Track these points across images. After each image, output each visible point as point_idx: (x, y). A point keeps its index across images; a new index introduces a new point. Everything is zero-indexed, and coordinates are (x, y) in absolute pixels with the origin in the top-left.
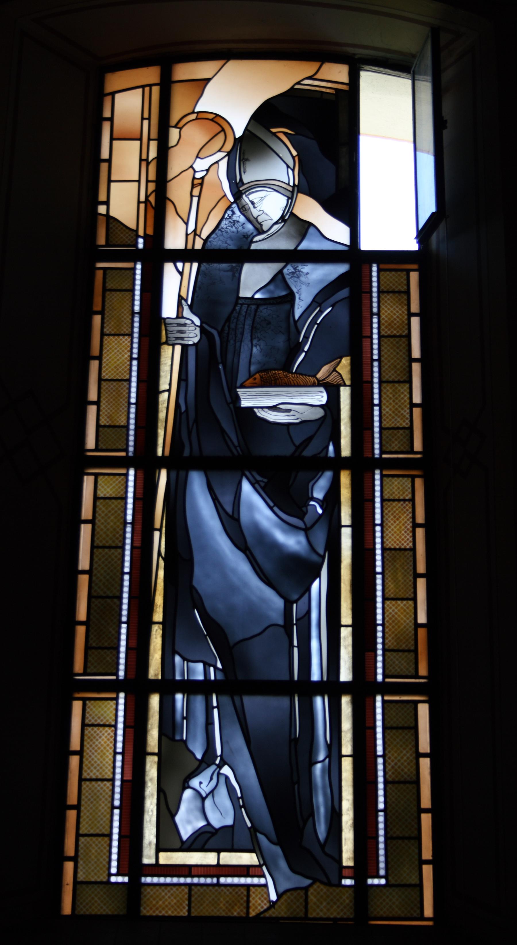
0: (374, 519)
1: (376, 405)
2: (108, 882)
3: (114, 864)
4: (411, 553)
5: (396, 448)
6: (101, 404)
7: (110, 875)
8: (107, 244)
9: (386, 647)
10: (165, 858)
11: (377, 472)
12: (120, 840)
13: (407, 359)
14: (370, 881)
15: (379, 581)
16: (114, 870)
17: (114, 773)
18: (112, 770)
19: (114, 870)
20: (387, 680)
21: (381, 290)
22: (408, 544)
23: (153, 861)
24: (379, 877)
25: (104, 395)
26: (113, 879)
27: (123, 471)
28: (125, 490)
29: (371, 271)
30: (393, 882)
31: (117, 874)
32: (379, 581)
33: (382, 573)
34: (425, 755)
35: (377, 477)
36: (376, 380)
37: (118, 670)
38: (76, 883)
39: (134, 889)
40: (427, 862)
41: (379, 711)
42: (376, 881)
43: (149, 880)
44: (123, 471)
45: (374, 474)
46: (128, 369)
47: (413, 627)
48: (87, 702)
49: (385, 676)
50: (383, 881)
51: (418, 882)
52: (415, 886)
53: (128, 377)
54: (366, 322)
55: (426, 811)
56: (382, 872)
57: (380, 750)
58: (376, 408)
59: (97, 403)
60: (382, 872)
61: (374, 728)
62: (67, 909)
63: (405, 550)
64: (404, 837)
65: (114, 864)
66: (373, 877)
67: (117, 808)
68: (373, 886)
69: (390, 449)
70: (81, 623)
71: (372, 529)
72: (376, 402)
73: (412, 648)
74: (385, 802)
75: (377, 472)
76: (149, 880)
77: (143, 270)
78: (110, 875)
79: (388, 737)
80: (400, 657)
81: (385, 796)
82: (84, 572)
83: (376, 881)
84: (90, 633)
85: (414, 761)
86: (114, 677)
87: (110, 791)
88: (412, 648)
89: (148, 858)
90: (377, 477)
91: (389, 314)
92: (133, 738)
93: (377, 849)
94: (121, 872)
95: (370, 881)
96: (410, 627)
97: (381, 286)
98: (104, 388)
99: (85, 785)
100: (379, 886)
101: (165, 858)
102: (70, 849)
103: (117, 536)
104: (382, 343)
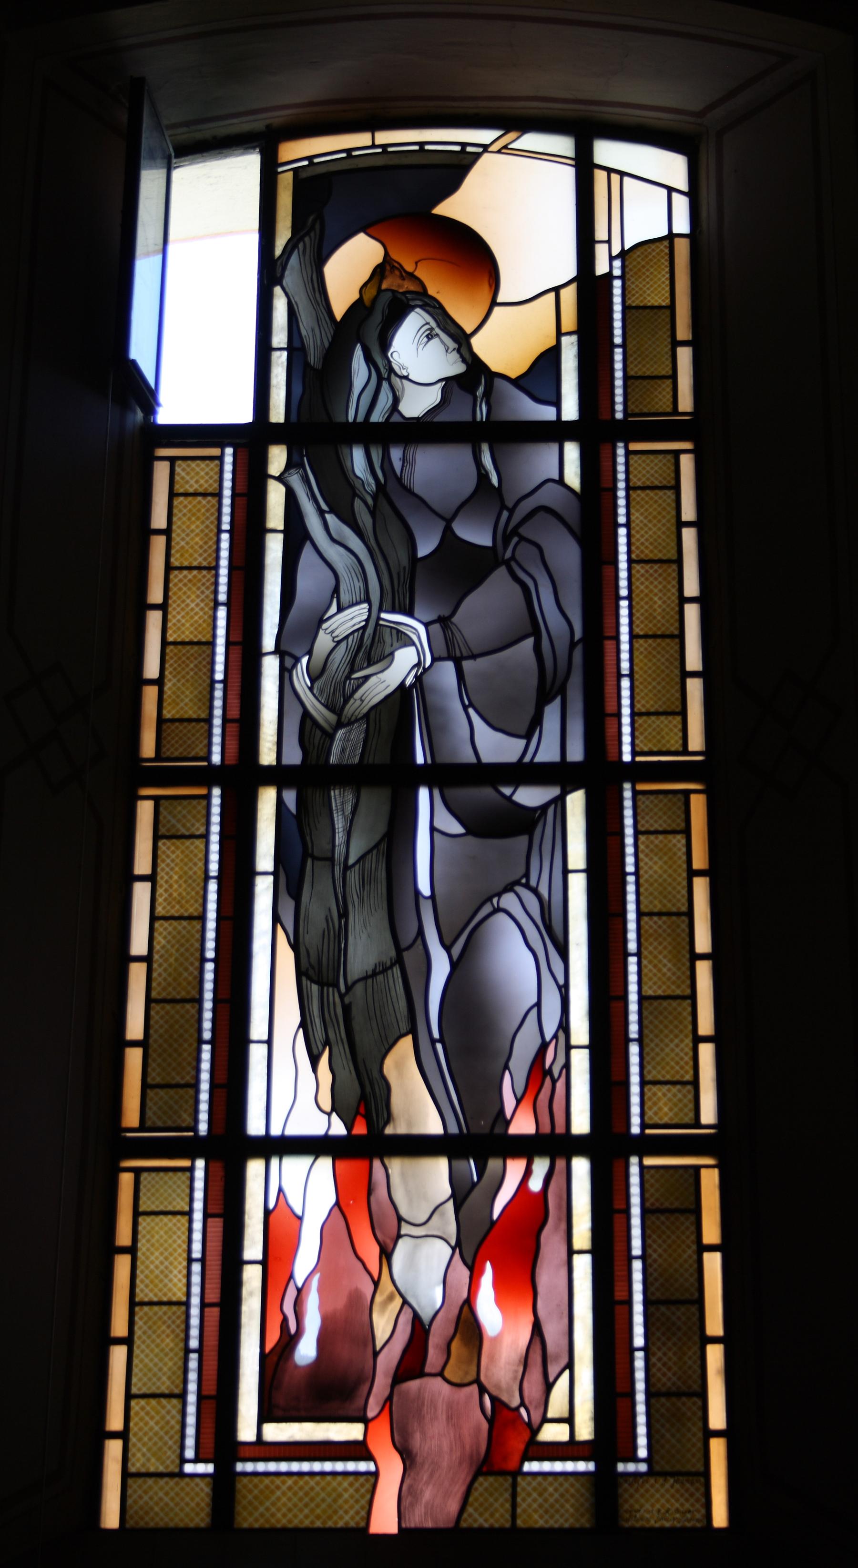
0: (617, 587)
1: (618, 346)
2: (182, 1475)
3: (190, 1442)
4: (668, 312)
5: (666, 1120)
6: (170, 609)
7: (183, 1461)
8: (158, 757)
9: (633, 556)
10: (275, 1432)
11: (627, 786)
12: (214, 1010)
13: (674, 521)
14: (621, 1467)
15: (633, 968)
16: (190, 1453)
17: (188, 1294)
18: (185, 1289)
19: (190, 1453)
20: (638, 759)
21: (636, 710)
22: (669, 497)
23: (262, 1132)
24: (636, 1459)
25: (174, 617)
26: (189, 1468)
27: (186, 1163)
28: (215, 547)
29: (614, 456)
30: (657, 1468)
31: (197, 1460)
32: (633, 968)
33: (638, 954)
34: (712, 1248)
35: (628, 794)
36: (621, 485)
37: (196, 1121)
38: (161, 721)
39: (224, 1483)
40: (694, 674)
41: (635, 1190)
42: (631, 1467)
43: (249, 1467)
44: (186, 1163)
45: (621, 791)
46: (211, 584)
47: (677, 601)
48: (137, 1300)
49: (634, 753)
50: (643, 1467)
51: (702, 1469)
52: (697, 1474)
53: (202, 830)
54: (609, 688)
55: (718, 1434)
56: (642, 1453)
57: (637, 1247)
58: (633, 960)
59: (151, 878)
60: (642, 1453)
61: (626, 1212)
62: (111, 1518)
63: (660, 307)
64: (679, 1395)
65: (190, 1442)
66: (626, 1460)
67: (207, 1042)
68: (626, 1475)
69: (656, 1120)
70: (134, 1044)
71: (615, 683)
72: (622, 520)
73: (684, 909)
74: (650, 1447)
75: (627, 786)
76: (249, 1467)
77: (223, 797)
78: (183, 1461)
79: (648, 1223)
80: (656, 571)
81: (649, 1436)
82: (134, 1044)
83: (631, 1467)
84: (149, 1070)
85: (695, 1257)
86: (206, 764)
87: (182, 1331)
88: (676, 632)
89: (246, 1432)
90: (628, 794)
91: (646, 611)
92: (216, 1358)
93: (612, 378)
94: (201, 1456)
95: (621, 1467)
96: (673, 601)
97: (636, 703)
98: (176, 580)
99: (143, 1221)
100: (636, 1475)
101: (275, 1432)
102: (119, 1327)
103: (192, 950)
104: (631, 462)
